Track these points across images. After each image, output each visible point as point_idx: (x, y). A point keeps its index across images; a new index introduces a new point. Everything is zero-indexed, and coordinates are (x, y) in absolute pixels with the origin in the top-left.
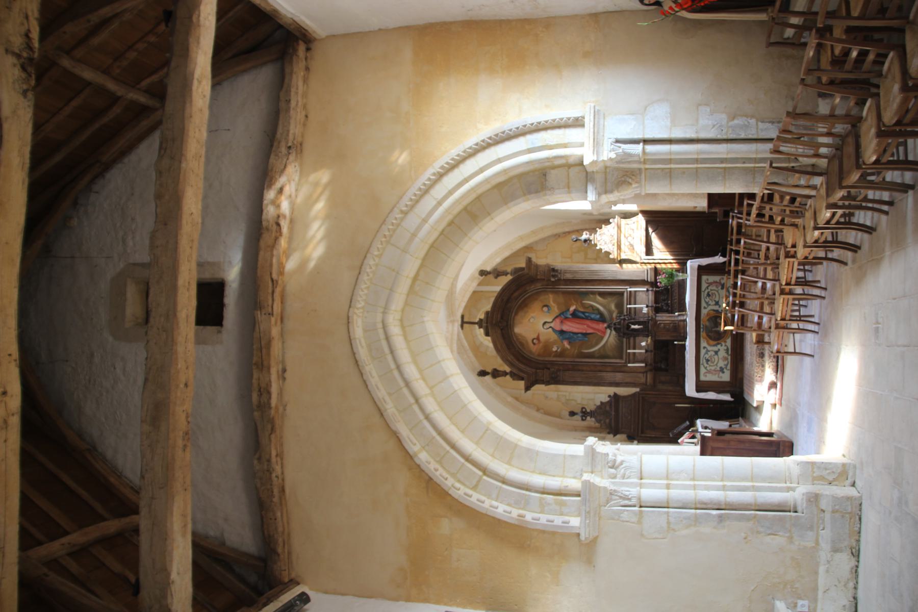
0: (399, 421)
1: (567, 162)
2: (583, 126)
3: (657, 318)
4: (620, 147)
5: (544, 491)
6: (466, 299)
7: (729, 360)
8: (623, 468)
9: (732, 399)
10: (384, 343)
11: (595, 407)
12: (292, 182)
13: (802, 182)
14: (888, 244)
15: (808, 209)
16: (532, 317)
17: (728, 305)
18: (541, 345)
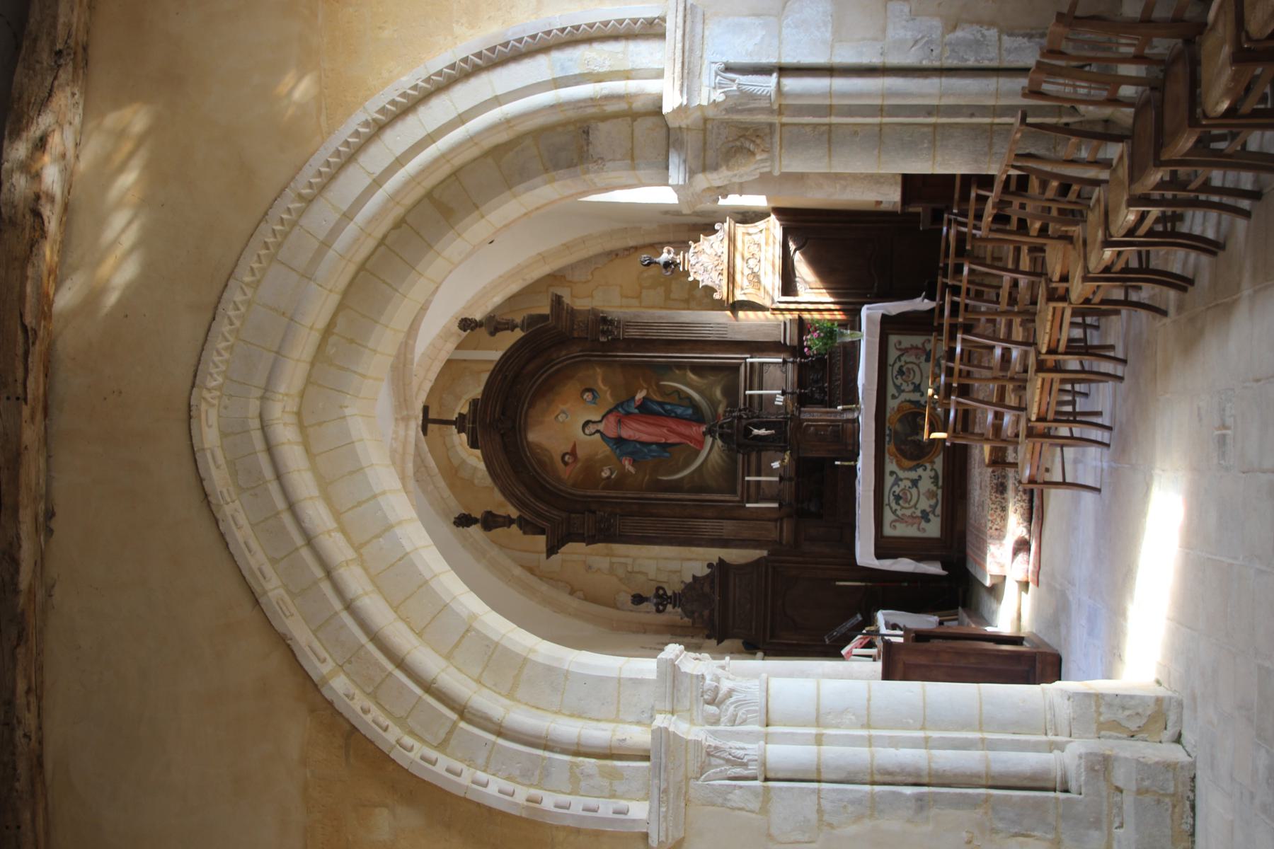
0: (292, 615)
1: (630, 108)
2: (662, 36)
3: (803, 416)
4: (733, 81)
5: (579, 750)
6: (433, 376)
7: (940, 497)
8: (732, 703)
9: (944, 573)
10: (263, 459)
11: (683, 586)
12: (66, 127)
13: (1084, 154)
14: (1247, 275)
15: (1094, 206)
16: (563, 412)
17: (937, 391)
18: (579, 465)
